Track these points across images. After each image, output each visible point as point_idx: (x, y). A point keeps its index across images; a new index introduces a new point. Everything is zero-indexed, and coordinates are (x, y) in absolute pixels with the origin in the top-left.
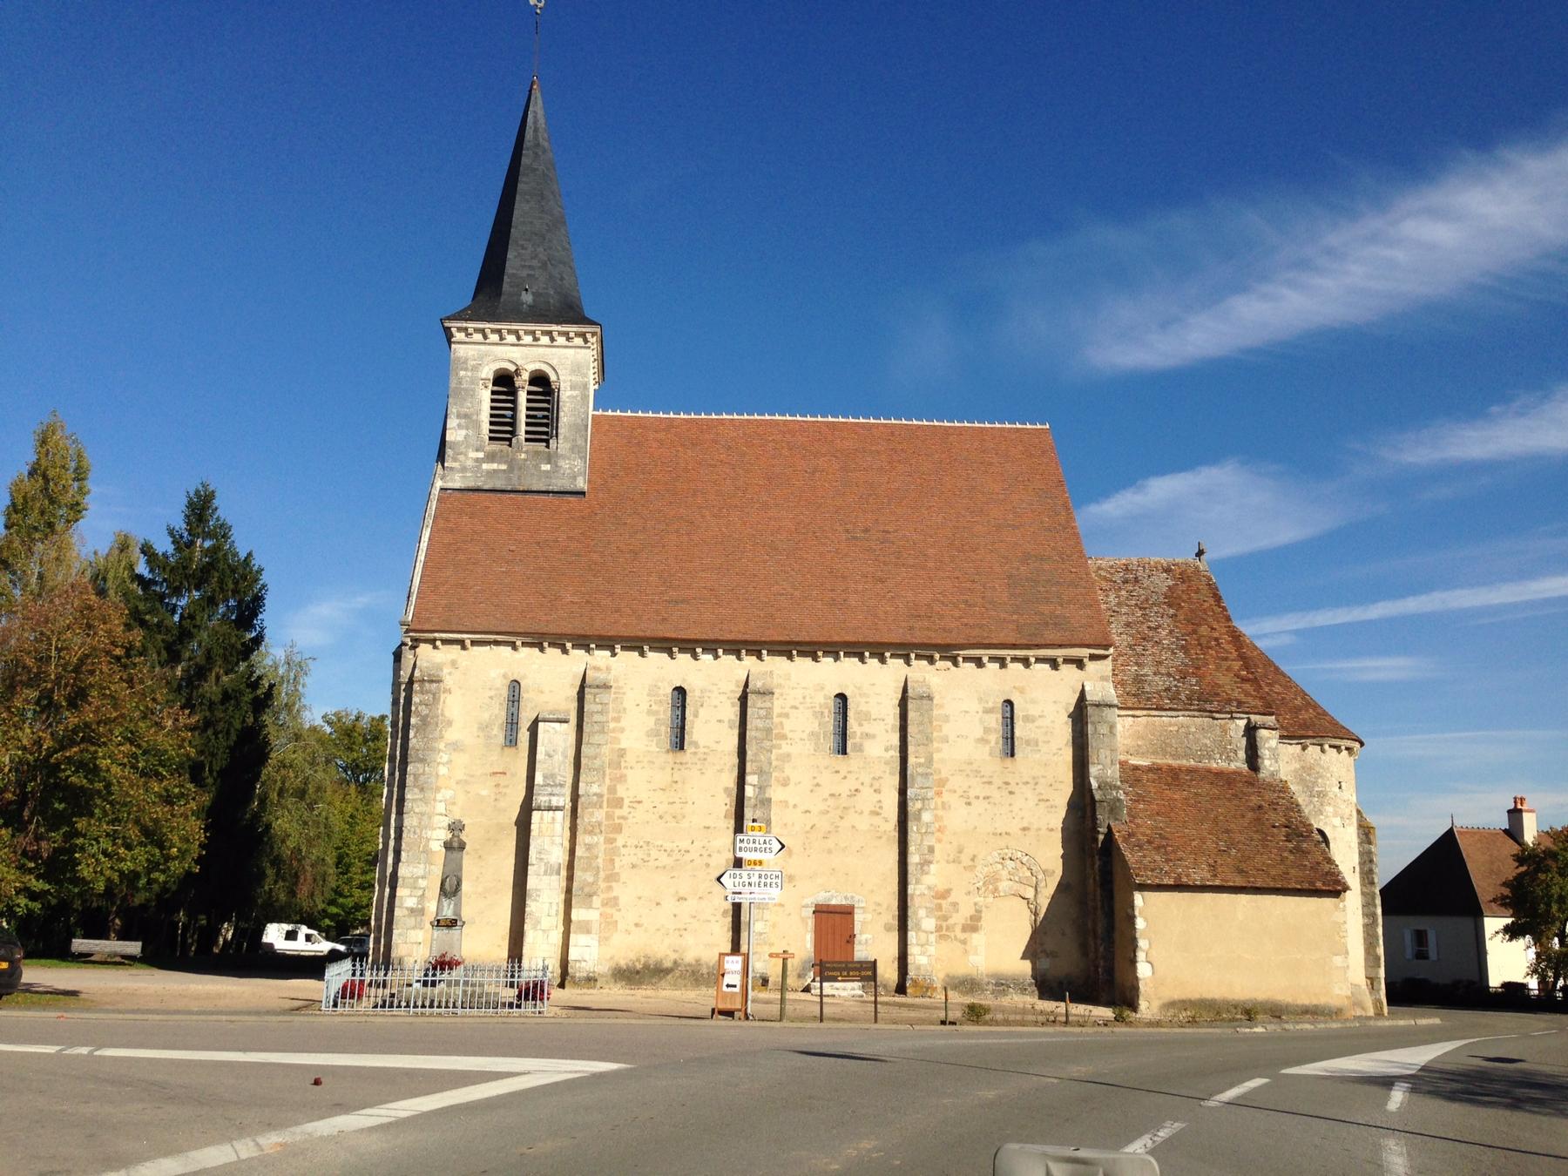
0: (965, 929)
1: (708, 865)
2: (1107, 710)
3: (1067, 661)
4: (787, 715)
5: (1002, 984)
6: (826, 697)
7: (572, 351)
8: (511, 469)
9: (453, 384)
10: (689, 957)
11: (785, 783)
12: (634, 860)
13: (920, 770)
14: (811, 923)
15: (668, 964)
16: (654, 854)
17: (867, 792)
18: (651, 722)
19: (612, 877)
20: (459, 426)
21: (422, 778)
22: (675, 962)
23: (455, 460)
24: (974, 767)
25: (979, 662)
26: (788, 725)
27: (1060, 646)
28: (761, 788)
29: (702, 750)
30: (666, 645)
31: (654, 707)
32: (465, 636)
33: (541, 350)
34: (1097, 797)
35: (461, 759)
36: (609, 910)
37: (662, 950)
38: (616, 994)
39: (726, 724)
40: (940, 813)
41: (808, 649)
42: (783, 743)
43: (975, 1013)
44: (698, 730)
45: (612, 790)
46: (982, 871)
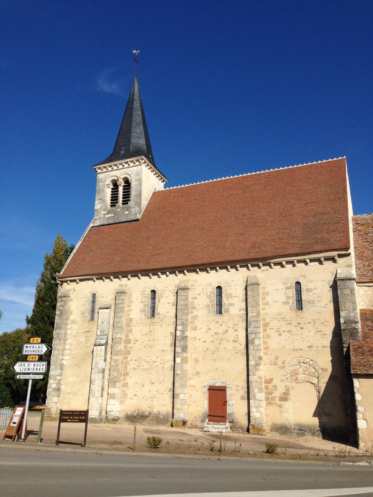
0: (281, 399)
1: (163, 368)
2: (348, 282)
3: (327, 259)
4: (196, 298)
5: (302, 430)
6: (212, 288)
7: (136, 168)
8: (115, 215)
9: (97, 189)
10: (155, 411)
11: (195, 329)
12: (134, 366)
13: (254, 319)
14: (207, 395)
15: (147, 414)
16: (142, 363)
17: (231, 331)
18: (142, 306)
19: (126, 374)
20: (99, 203)
21: (60, 335)
22: (150, 413)
23: (97, 215)
24: (282, 316)
25: (281, 264)
26: (196, 302)
27: (321, 252)
28: (183, 331)
29: (161, 316)
30: (146, 273)
31: (144, 300)
32: (76, 278)
33: (125, 170)
34: (342, 327)
35: (75, 327)
36: (125, 389)
37: (144, 407)
38: (127, 428)
39: (171, 304)
40: (266, 340)
41: (202, 267)
42: (194, 311)
43: (155, 444)
44: (161, 308)
45: (127, 336)
46: (288, 369)
